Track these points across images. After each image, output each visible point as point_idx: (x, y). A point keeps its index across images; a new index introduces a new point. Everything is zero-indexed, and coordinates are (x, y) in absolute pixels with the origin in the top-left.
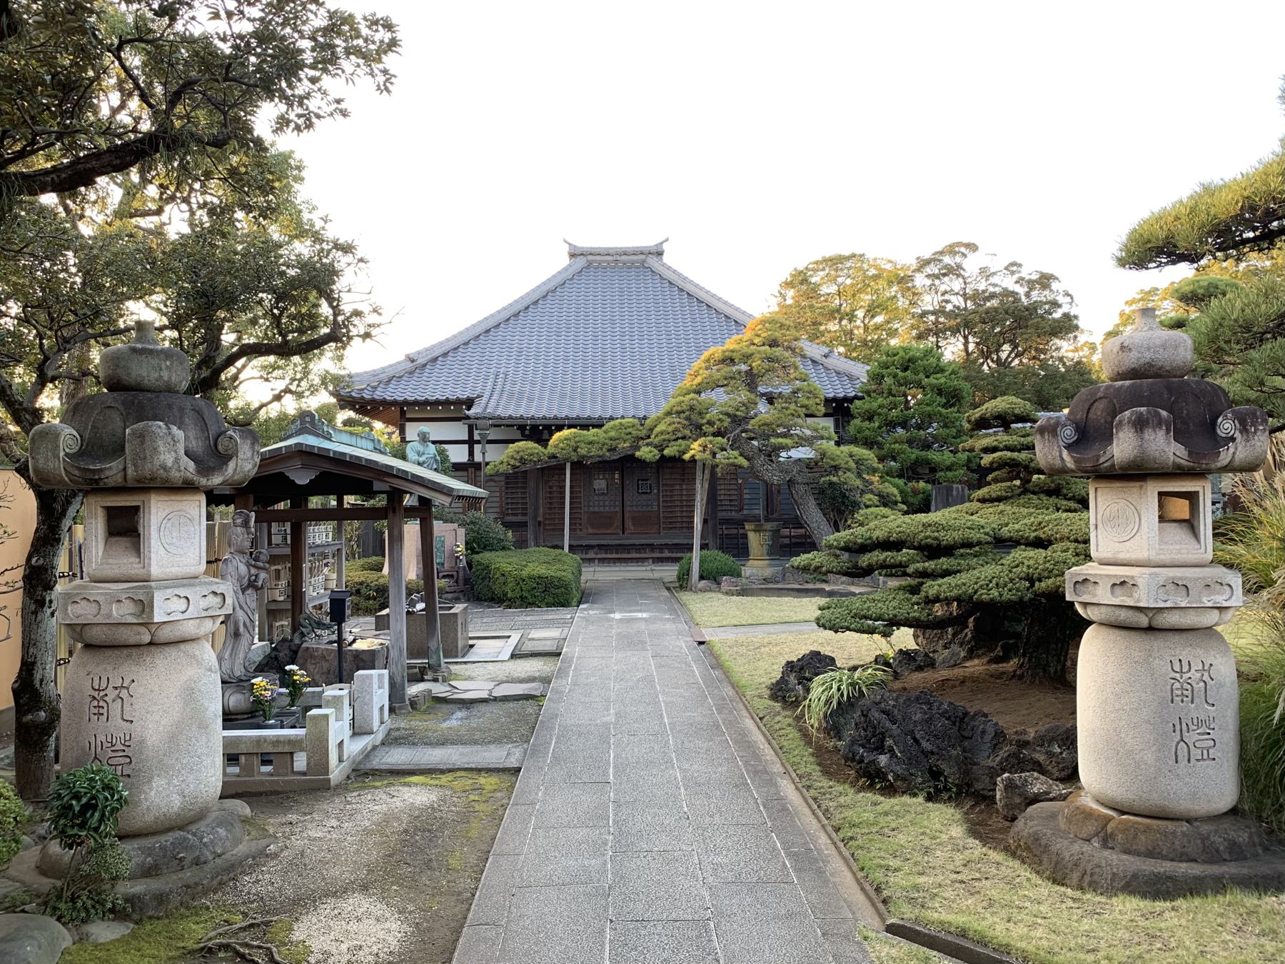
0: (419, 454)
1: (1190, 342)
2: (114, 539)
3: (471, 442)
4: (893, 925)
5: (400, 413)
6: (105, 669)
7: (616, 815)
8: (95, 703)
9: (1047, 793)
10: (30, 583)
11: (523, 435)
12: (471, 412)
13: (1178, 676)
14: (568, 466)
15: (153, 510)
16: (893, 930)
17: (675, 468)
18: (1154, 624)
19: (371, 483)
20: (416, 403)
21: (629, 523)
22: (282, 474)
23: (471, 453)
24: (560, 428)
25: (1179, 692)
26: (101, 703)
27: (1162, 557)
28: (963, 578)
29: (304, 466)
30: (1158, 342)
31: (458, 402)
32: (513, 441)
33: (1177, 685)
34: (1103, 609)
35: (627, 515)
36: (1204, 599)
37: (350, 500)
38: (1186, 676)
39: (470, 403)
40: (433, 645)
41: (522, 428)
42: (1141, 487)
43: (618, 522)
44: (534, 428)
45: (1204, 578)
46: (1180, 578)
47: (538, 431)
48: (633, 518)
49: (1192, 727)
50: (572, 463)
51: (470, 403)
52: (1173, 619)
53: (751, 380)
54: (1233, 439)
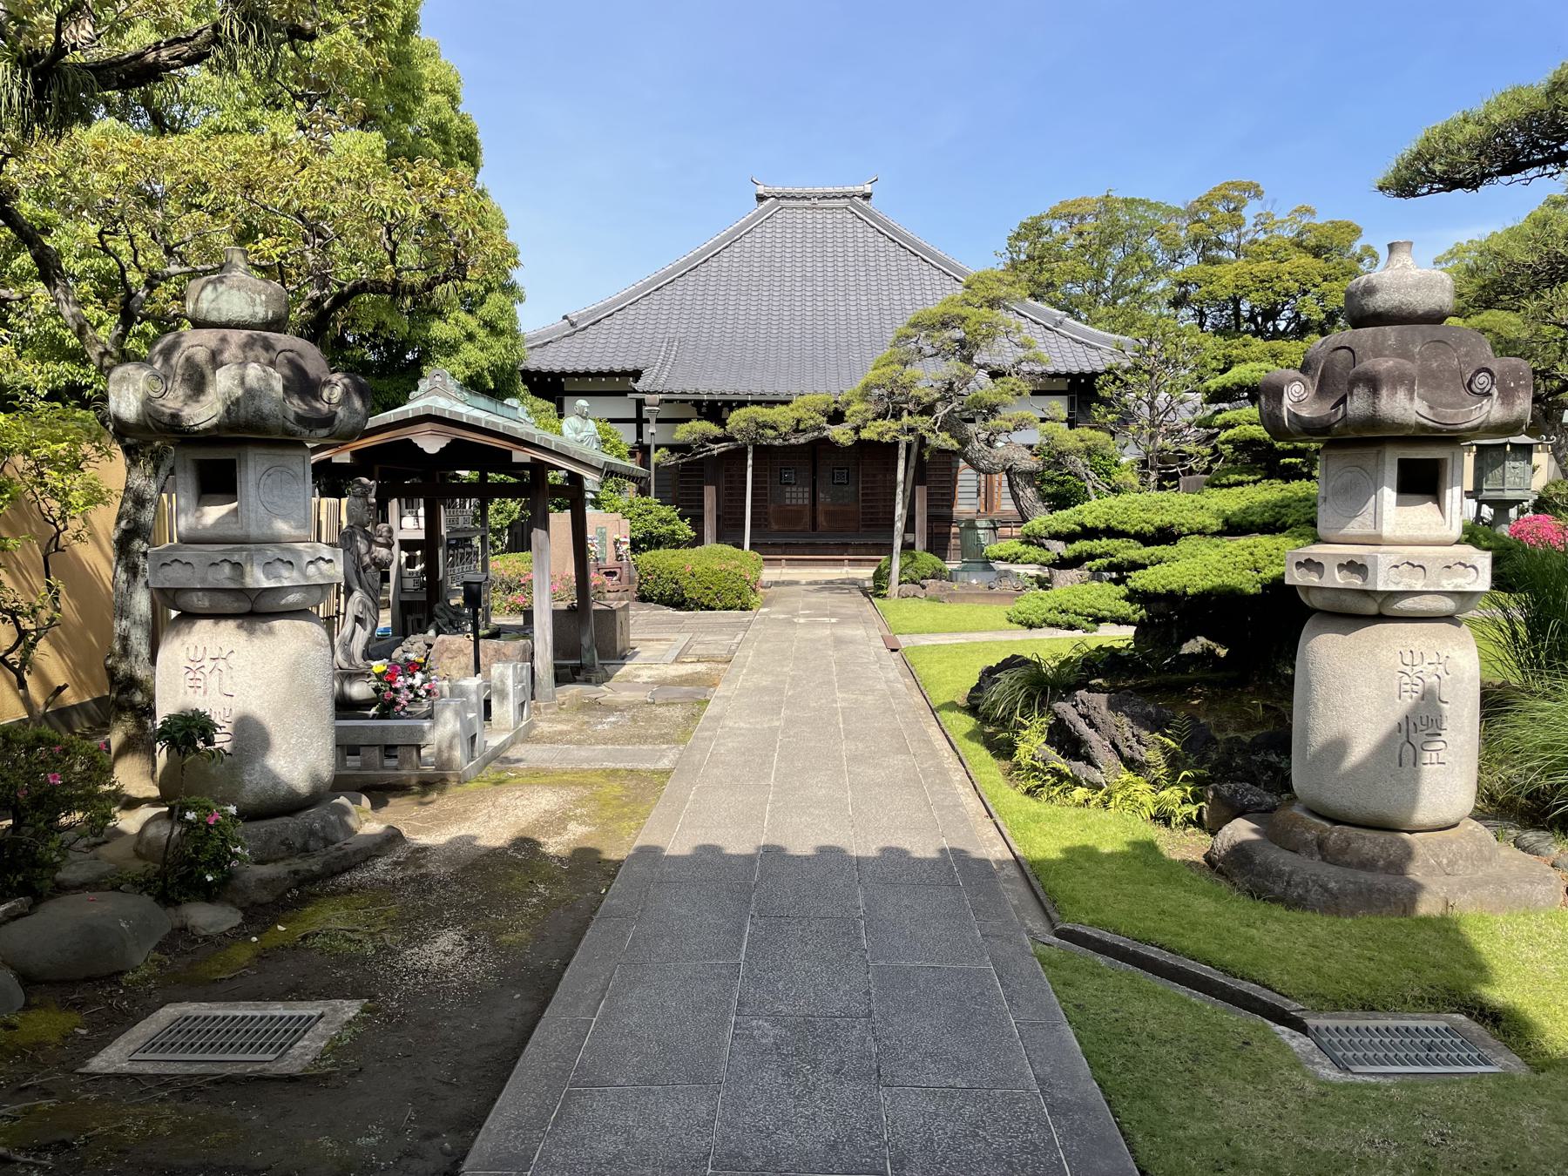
0: (576, 431)
1: (1449, 282)
2: (207, 497)
3: (640, 421)
4: (1062, 930)
5: (552, 388)
6: (202, 640)
7: (772, 816)
8: (191, 675)
9: (1259, 804)
10: (474, 865)
11: (699, 413)
12: (639, 386)
13: (1408, 669)
14: (750, 449)
15: (251, 464)
16: (1061, 934)
17: (879, 454)
18: (1387, 612)
19: (510, 453)
20: (575, 374)
21: (821, 519)
22: (408, 443)
23: (640, 434)
24: (742, 404)
25: (1408, 687)
26: (199, 675)
27: (1398, 533)
28: (1179, 567)
29: (435, 433)
30: (1410, 281)
31: (624, 374)
32: (687, 420)
33: (1406, 679)
34: (1327, 594)
35: (820, 508)
36: (1444, 582)
37: (495, 477)
38: (1416, 669)
39: (637, 374)
40: (586, 641)
41: (698, 404)
42: (1379, 453)
43: (807, 519)
44: (713, 403)
45: (1445, 558)
46: (1416, 558)
47: (714, 410)
48: (826, 513)
49: (1420, 727)
50: (755, 447)
51: (637, 374)
52: (1407, 604)
53: (965, 350)
54: (1488, 394)
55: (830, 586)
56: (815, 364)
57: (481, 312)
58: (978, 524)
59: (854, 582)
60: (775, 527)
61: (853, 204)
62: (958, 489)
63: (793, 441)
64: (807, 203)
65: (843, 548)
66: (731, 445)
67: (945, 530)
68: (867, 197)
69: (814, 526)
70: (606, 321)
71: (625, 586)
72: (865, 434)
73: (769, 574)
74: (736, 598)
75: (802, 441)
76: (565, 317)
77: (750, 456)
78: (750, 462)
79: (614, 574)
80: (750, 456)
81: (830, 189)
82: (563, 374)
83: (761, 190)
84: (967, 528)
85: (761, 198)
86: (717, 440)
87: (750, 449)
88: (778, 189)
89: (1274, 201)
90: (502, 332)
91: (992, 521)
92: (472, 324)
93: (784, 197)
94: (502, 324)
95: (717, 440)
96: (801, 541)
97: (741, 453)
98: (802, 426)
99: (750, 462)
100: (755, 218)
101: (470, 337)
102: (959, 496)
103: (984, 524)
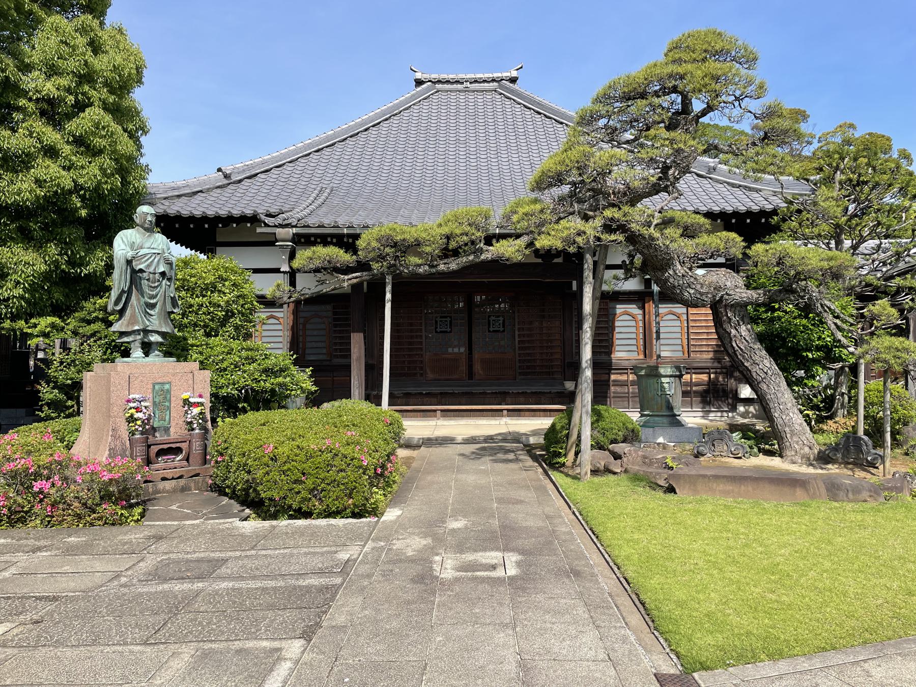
14: (389, 279)
21: (478, 367)
35: (476, 356)
43: (463, 368)
55: (490, 447)
56: (468, 183)
57: (72, 126)
58: (662, 371)
59: (516, 438)
60: (430, 376)
61: (501, 87)
62: (617, 336)
63: (442, 267)
64: (459, 86)
65: (502, 397)
66: (365, 276)
67: (605, 377)
68: (513, 80)
69: (471, 375)
70: (262, 176)
71: (195, 468)
72: (543, 242)
73: (416, 428)
74: (348, 491)
75: (453, 266)
76: (219, 170)
77: (389, 288)
78: (388, 296)
79: (178, 451)
80: (389, 288)
81: (478, 76)
82: (217, 219)
83: (419, 75)
84: (647, 376)
85: (419, 83)
86: (346, 270)
87: (389, 279)
88: (433, 76)
89: (815, 125)
90: (100, 152)
91: (678, 368)
92: (52, 136)
93: (439, 82)
94: (98, 142)
95: (346, 270)
96: (457, 390)
97: (377, 286)
98: (453, 245)
99: (388, 296)
100: (413, 97)
101: (51, 152)
102: (617, 342)
103: (669, 371)
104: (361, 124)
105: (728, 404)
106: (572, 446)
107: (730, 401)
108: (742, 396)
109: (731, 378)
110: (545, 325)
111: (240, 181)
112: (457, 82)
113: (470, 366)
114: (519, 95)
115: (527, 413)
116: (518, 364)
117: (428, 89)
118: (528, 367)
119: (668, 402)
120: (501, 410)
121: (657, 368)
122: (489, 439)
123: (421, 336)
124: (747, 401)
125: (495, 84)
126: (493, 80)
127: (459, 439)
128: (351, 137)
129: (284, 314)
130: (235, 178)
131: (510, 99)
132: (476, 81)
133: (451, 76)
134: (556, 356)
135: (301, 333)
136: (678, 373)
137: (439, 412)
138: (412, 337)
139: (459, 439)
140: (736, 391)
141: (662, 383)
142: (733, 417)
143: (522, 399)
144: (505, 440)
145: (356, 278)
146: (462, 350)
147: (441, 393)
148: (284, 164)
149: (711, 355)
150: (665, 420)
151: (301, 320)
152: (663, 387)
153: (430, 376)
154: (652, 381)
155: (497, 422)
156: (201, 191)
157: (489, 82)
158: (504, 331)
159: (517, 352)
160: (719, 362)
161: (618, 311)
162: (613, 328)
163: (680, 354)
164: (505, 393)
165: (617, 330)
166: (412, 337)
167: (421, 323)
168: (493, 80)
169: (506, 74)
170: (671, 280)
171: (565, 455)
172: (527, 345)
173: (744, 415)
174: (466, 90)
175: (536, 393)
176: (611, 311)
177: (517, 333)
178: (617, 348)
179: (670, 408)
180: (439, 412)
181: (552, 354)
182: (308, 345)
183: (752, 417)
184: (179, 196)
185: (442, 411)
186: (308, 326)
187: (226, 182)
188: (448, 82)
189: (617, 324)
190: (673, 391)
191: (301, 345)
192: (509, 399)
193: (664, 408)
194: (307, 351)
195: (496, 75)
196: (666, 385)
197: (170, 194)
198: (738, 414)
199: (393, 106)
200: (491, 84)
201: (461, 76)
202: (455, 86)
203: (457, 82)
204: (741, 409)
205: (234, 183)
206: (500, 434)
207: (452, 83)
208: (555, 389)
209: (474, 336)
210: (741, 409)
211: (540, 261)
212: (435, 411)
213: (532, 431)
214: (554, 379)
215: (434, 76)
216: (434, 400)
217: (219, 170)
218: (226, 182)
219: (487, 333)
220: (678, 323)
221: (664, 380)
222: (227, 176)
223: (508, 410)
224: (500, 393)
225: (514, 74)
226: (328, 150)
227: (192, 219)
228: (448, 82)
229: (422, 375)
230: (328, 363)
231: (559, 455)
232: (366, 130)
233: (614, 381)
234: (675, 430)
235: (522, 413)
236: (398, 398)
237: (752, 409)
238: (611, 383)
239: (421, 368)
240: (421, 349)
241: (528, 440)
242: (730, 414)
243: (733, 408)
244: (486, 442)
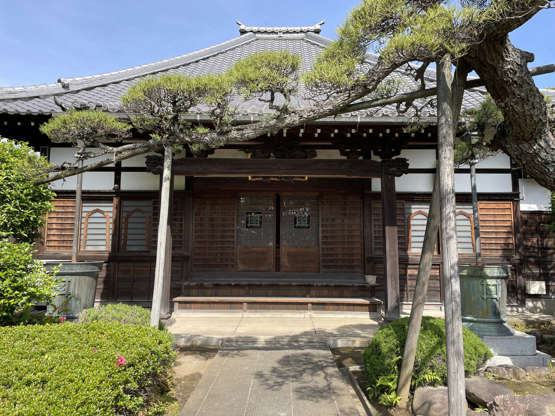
21: (284, 260)
35: (283, 250)
43: (271, 260)
58: (488, 271)
59: (320, 340)
60: (241, 267)
61: (307, 36)
62: (413, 234)
64: (275, 36)
65: (306, 289)
68: (317, 32)
69: (278, 267)
76: (59, 81)
83: (243, 27)
85: (243, 32)
93: (259, 32)
96: (265, 281)
102: (413, 239)
104: (193, 57)
105: (517, 300)
106: (407, 380)
107: (519, 296)
108: (532, 292)
109: (519, 275)
110: (346, 222)
111: (78, 91)
112: (273, 32)
113: (278, 259)
114: (322, 41)
115: (331, 307)
116: (321, 258)
117: (250, 37)
118: (331, 261)
119: (495, 307)
120: (306, 304)
121: (482, 268)
122: (293, 341)
123: (233, 230)
124: (536, 297)
125: (303, 34)
126: (302, 32)
127: (262, 340)
128: (184, 65)
129: (109, 209)
130: (72, 88)
131: (315, 44)
132: (288, 32)
133: (269, 29)
134: (357, 251)
135: (123, 226)
136: (505, 275)
137: (245, 304)
138: (224, 231)
139: (262, 340)
140: (525, 287)
141: (487, 285)
142: (523, 312)
143: (325, 292)
144: (311, 344)
145: (128, 149)
146: (271, 244)
147: (249, 285)
148: (121, 81)
149: (500, 253)
150: (492, 328)
151: (124, 215)
152: (488, 290)
153: (241, 267)
154: (476, 283)
155: (302, 316)
156: (38, 97)
157: (298, 33)
158: (309, 227)
159: (321, 246)
160: (508, 260)
161: (413, 211)
162: (409, 226)
163: (471, 251)
164: (310, 286)
165: (413, 228)
166: (224, 231)
167: (233, 218)
168: (302, 32)
169: (312, 28)
170: (543, 154)
171: (397, 391)
172: (329, 240)
173: (533, 310)
174: (280, 39)
175: (339, 286)
176: (407, 211)
177: (321, 229)
178: (413, 245)
179: (497, 314)
180: (245, 304)
181: (352, 248)
182: (129, 237)
183: (540, 312)
184: (15, 99)
185: (248, 303)
186: (130, 220)
187: (63, 91)
188: (266, 32)
189: (412, 222)
190: (500, 294)
191: (123, 237)
192: (313, 292)
193: (490, 314)
194: (128, 243)
195: (305, 28)
196: (493, 288)
197: (6, 97)
198: (527, 309)
199: (220, 46)
200: (300, 34)
201: (276, 29)
202: (271, 36)
203: (273, 32)
204: (530, 304)
205: (72, 92)
206: (305, 334)
207: (269, 33)
208: (357, 282)
209: (283, 232)
210: (530, 304)
211: (345, 158)
212: (241, 303)
213: (339, 329)
214: (354, 272)
215: (255, 29)
216: (242, 291)
217: (59, 81)
218: (63, 91)
219: (293, 229)
220: (468, 223)
221: (489, 282)
222: (65, 86)
223: (313, 304)
224: (305, 285)
225: (318, 27)
226: (162, 73)
227: (17, 116)
228: (266, 32)
229: (232, 266)
230: (146, 254)
231: (385, 389)
232: (197, 62)
233: (410, 275)
234: (506, 340)
235: (327, 307)
236: (208, 288)
237: (539, 304)
238: (408, 277)
239: (233, 260)
240: (233, 242)
241: (336, 344)
242: (520, 309)
243: (523, 303)
244: (291, 347)
